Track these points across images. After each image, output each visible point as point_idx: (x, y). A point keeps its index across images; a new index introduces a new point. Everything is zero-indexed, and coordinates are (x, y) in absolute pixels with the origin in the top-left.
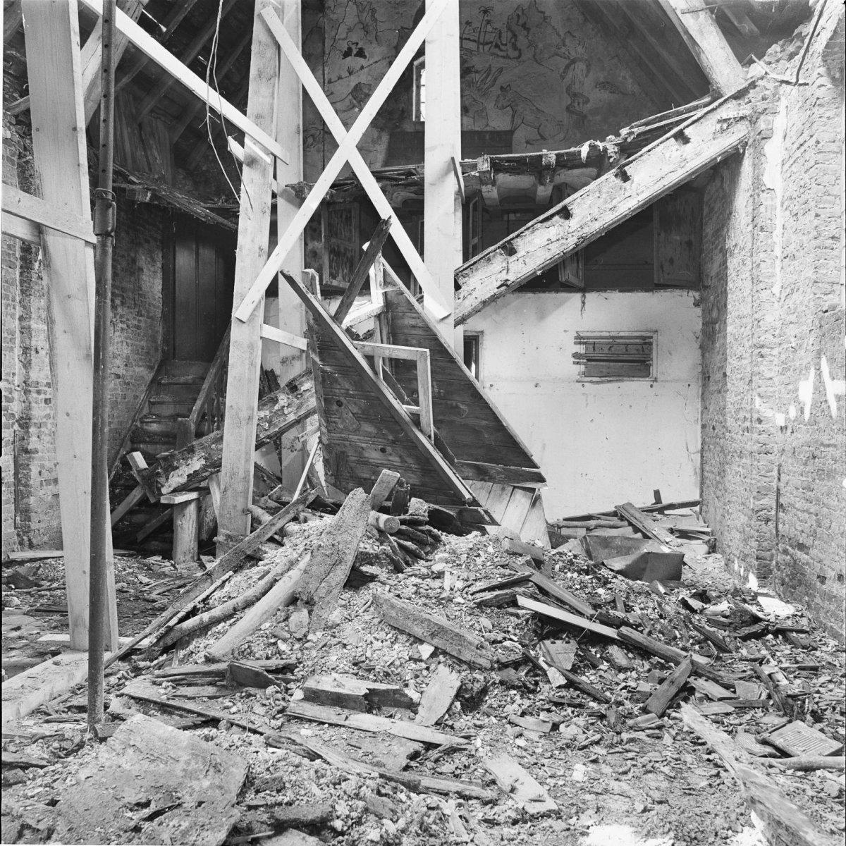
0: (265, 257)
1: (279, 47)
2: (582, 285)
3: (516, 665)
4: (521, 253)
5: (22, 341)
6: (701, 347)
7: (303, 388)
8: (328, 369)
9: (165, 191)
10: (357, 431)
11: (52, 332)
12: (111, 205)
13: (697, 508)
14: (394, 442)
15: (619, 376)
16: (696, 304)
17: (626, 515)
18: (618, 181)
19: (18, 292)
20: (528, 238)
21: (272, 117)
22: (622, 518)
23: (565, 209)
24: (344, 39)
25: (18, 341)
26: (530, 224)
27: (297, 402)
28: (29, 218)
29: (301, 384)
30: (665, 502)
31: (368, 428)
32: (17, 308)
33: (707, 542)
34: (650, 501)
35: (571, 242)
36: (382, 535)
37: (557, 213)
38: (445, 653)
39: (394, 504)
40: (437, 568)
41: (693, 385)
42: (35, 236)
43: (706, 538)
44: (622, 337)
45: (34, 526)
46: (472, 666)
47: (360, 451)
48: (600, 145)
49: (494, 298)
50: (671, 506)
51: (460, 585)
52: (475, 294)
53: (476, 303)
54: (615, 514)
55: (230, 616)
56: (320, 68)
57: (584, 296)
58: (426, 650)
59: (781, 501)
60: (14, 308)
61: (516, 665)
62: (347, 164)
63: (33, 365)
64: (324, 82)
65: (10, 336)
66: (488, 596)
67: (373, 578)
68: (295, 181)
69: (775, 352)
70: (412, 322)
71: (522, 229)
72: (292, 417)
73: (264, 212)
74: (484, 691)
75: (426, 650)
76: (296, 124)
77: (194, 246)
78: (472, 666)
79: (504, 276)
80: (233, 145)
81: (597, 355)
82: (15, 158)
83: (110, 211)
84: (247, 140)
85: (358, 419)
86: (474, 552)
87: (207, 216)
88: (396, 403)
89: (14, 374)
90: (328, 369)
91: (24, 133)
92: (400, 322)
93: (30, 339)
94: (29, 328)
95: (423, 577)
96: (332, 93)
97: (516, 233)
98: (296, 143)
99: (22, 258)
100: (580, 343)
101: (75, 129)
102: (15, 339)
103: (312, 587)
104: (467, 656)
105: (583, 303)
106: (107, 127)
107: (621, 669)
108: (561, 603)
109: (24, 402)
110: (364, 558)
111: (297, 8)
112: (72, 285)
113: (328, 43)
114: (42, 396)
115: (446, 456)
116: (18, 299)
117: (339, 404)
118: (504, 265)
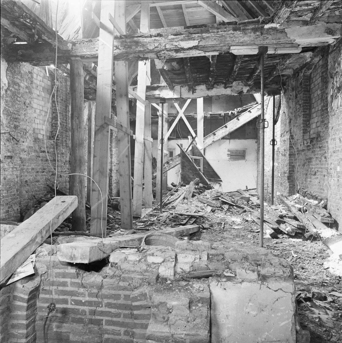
3: (219, 207)
8: (184, 160)
10: (188, 172)
13: (256, 190)
15: (238, 159)
16: (256, 143)
17: (239, 192)
20: (218, 132)
22: (238, 192)
23: (226, 126)
26: (218, 129)
30: (248, 188)
33: (257, 197)
34: (245, 189)
35: (227, 133)
36: (196, 189)
38: (209, 205)
39: (197, 184)
40: (206, 194)
43: (257, 196)
45: (113, 192)
46: (213, 207)
47: (189, 176)
48: (233, 112)
49: (211, 144)
50: (250, 190)
51: (210, 197)
53: (207, 145)
54: (237, 191)
55: (174, 201)
58: (206, 205)
59: (268, 186)
61: (219, 207)
62: (181, 117)
66: (214, 198)
67: (196, 195)
72: (168, 169)
74: (215, 210)
75: (206, 205)
78: (213, 207)
79: (213, 140)
86: (211, 192)
92: (195, 151)
95: (204, 196)
103: (187, 196)
104: (212, 205)
107: (235, 209)
108: (226, 200)
110: (194, 192)
115: (205, 176)
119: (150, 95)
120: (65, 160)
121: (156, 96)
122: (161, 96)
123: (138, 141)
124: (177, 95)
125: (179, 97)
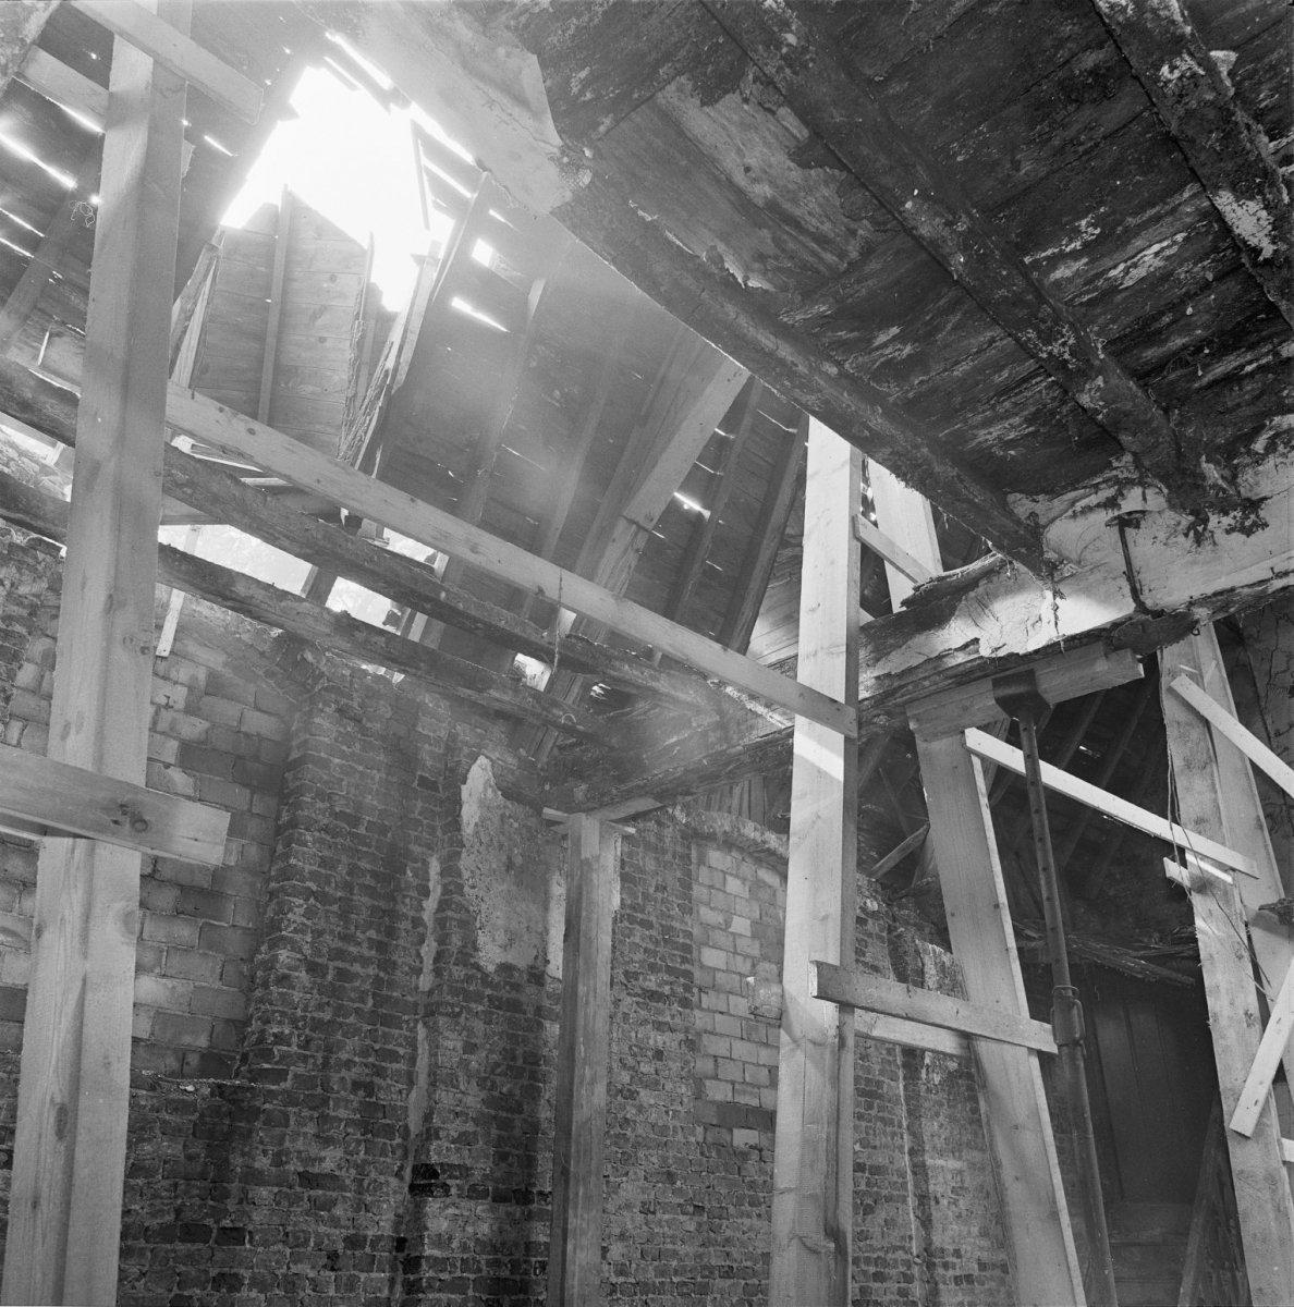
0: (1258, 1026)
1: (1207, 723)
5: (916, 1186)
9: (1076, 943)
11: (999, 1180)
12: (1074, 1004)
19: (904, 1114)
21: (1220, 818)
24: (1284, 671)
25: (910, 1187)
28: (954, 1026)
32: (905, 1137)
42: (963, 1048)
56: (1258, 718)
60: (902, 1138)
63: (934, 1221)
64: (1269, 738)
65: (900, 1180)
68: (1272, 899)
73: (1240, 958)
76: (1254, 816)
77: (1122, 1013)
80: (1172, 869)
82: (884, 934)
83: (1075, 1011)
84: (1189, 857)
87: (1143, 969)
89: (911, 1238)
91: (889, 899)
93: (926, 1182)
94: (923, 1165)
96: (1286, 749)
98: (1261, 844)
99: (905, 1065)
101: (997, 906)
102: (906, 1183)
106: (1052, 907)
109: (928, 1282)
111: (1218, 664)
112: (1020, 1112)
113: (1261, 684)
114: (951, 1273)
116: (905, 1124)
119: (910, 670)
120: (338, 1234)
121: (951, 662)
122: (985, 651)
123: (798, 1033)
124: (1106, 600)
125: (1126, 608)
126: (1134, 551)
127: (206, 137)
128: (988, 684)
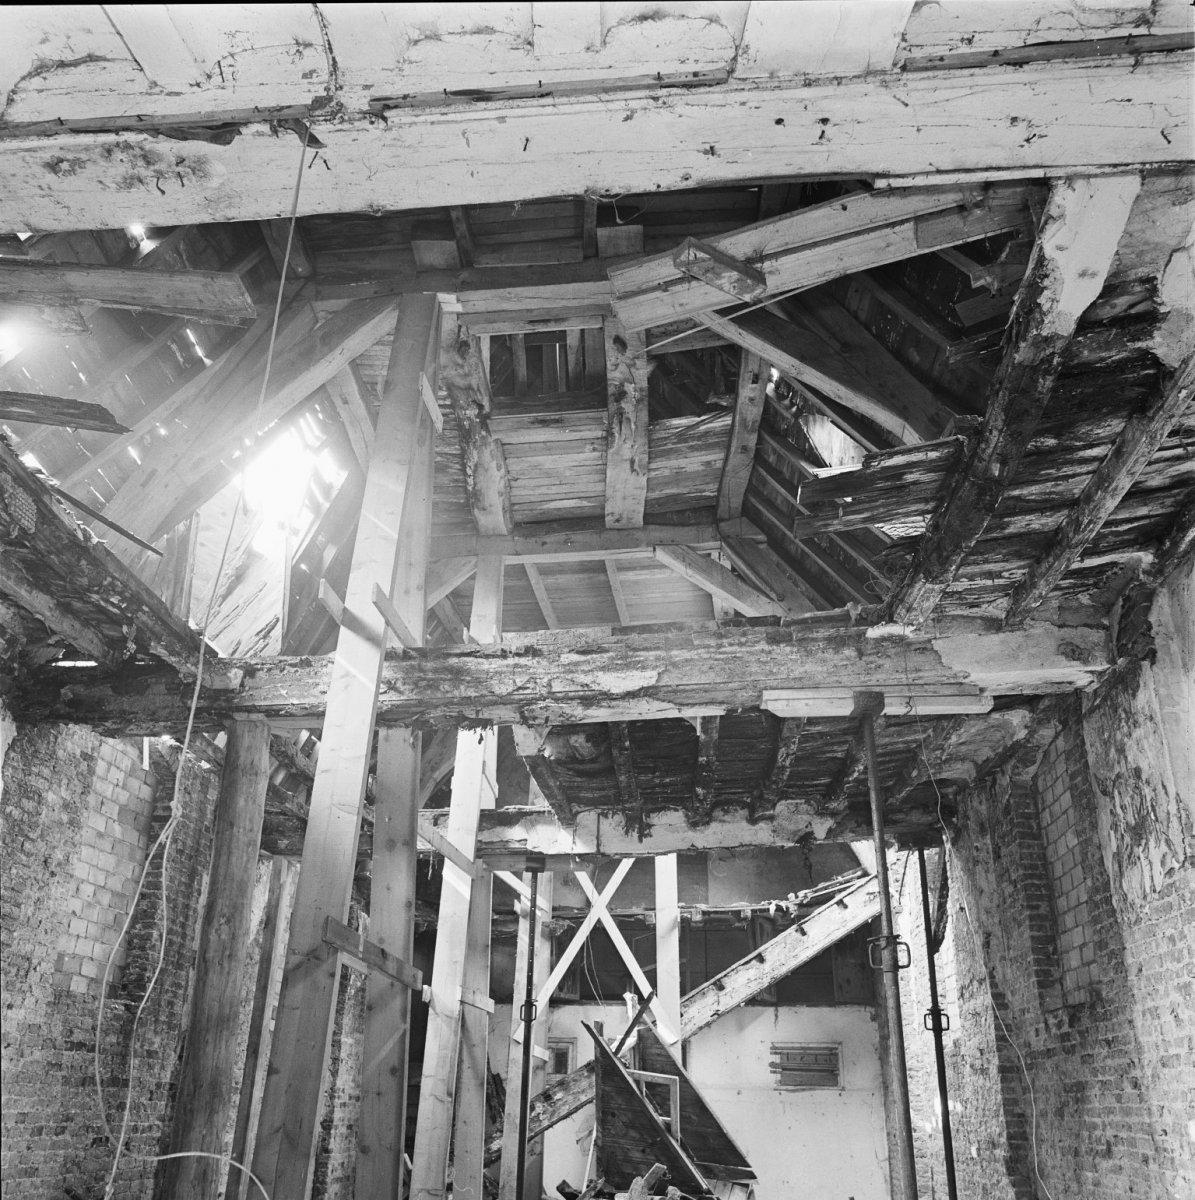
2: (774, 1000)
4: (728, 989)
5: (333, 1053)
6: (880, 1059)
7: (556, 1098)
10: (625, 1136)
14: (652, 1144)
18: (798, 935)
26: (734, 966)
27: (551, 1109)
29: (555, 1093)
31: (633, 1133)
35: (766, 982)
37: (754, 958)
41: (877, 1094)
44: (811, 1049)
48: (783, 904)
49: (708, 1025)
52: (694, 1021)
53: (695, 1028)
57: (777, 1010)
62: (599, 921)
69: (920, 1074)
70: (658, 1051)
71: (729, 970)
79: (715, 1007)
81: (791, 1066)
85: (627, 1127)
88: (655, 1115)
90: (607, 1088)
97: (724, 973)
100: (776, 1053)
105: (776, 1016)
115: (689, 1156)
117: (613, 1115)
118: (716, 998)
119: (492, 843)
121: (512, 846)
122: (529, 847)
126: (601, 826)
127: (130, 448)
128: (524, 858)
